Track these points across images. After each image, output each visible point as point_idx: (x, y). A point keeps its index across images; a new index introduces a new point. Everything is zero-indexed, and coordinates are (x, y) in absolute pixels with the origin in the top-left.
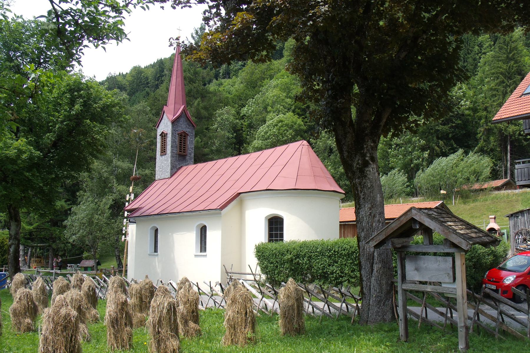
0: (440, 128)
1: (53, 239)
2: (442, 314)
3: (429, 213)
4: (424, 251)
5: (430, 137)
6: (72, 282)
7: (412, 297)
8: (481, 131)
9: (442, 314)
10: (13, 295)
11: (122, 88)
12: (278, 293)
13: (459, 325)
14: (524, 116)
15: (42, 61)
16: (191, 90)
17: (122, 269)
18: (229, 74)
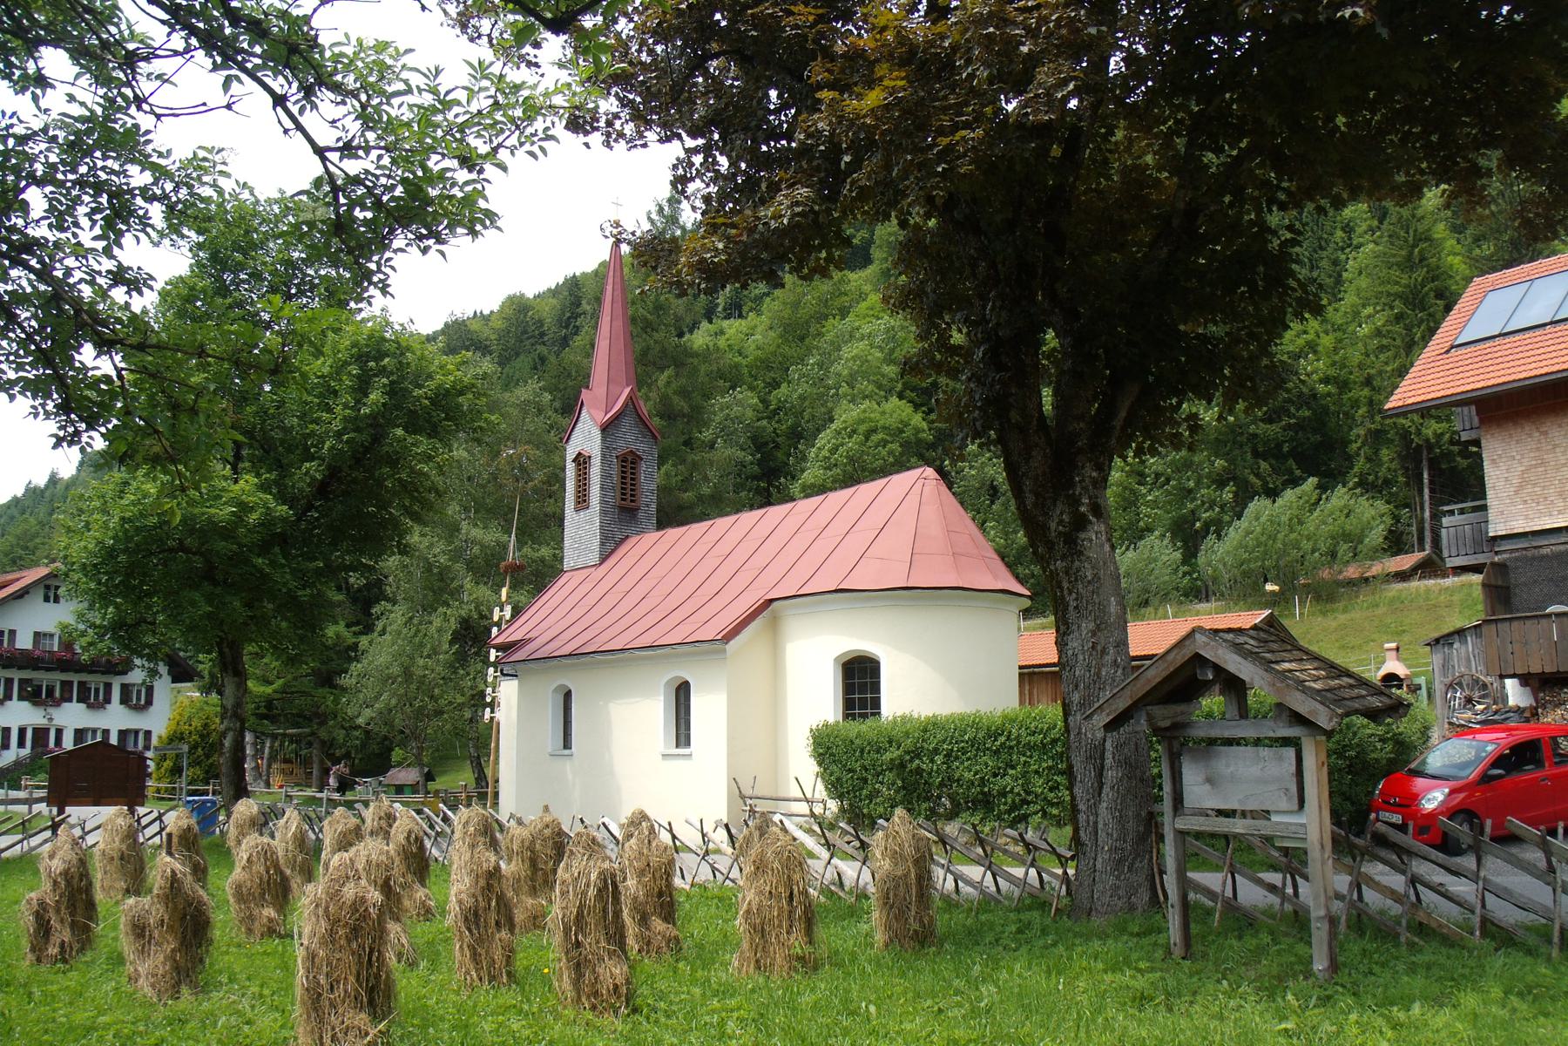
0: (1261, 429)
1: (322, 719)
2: (1272, 888)
3: (1237, 641)
4: (1227, 734)
5: (1237, 452)
6: (369, 821)
7: (1200, 849)
8: (1358, 436)
9: (1272, 888)
10: (233, 851)
11: (481, 347)
12: (869, 846)
13: (1313, 915)
14: (1459, 398)
15: (293, 291)
16: (648, 348)
17: (485, 790)
18: (739, 307)
